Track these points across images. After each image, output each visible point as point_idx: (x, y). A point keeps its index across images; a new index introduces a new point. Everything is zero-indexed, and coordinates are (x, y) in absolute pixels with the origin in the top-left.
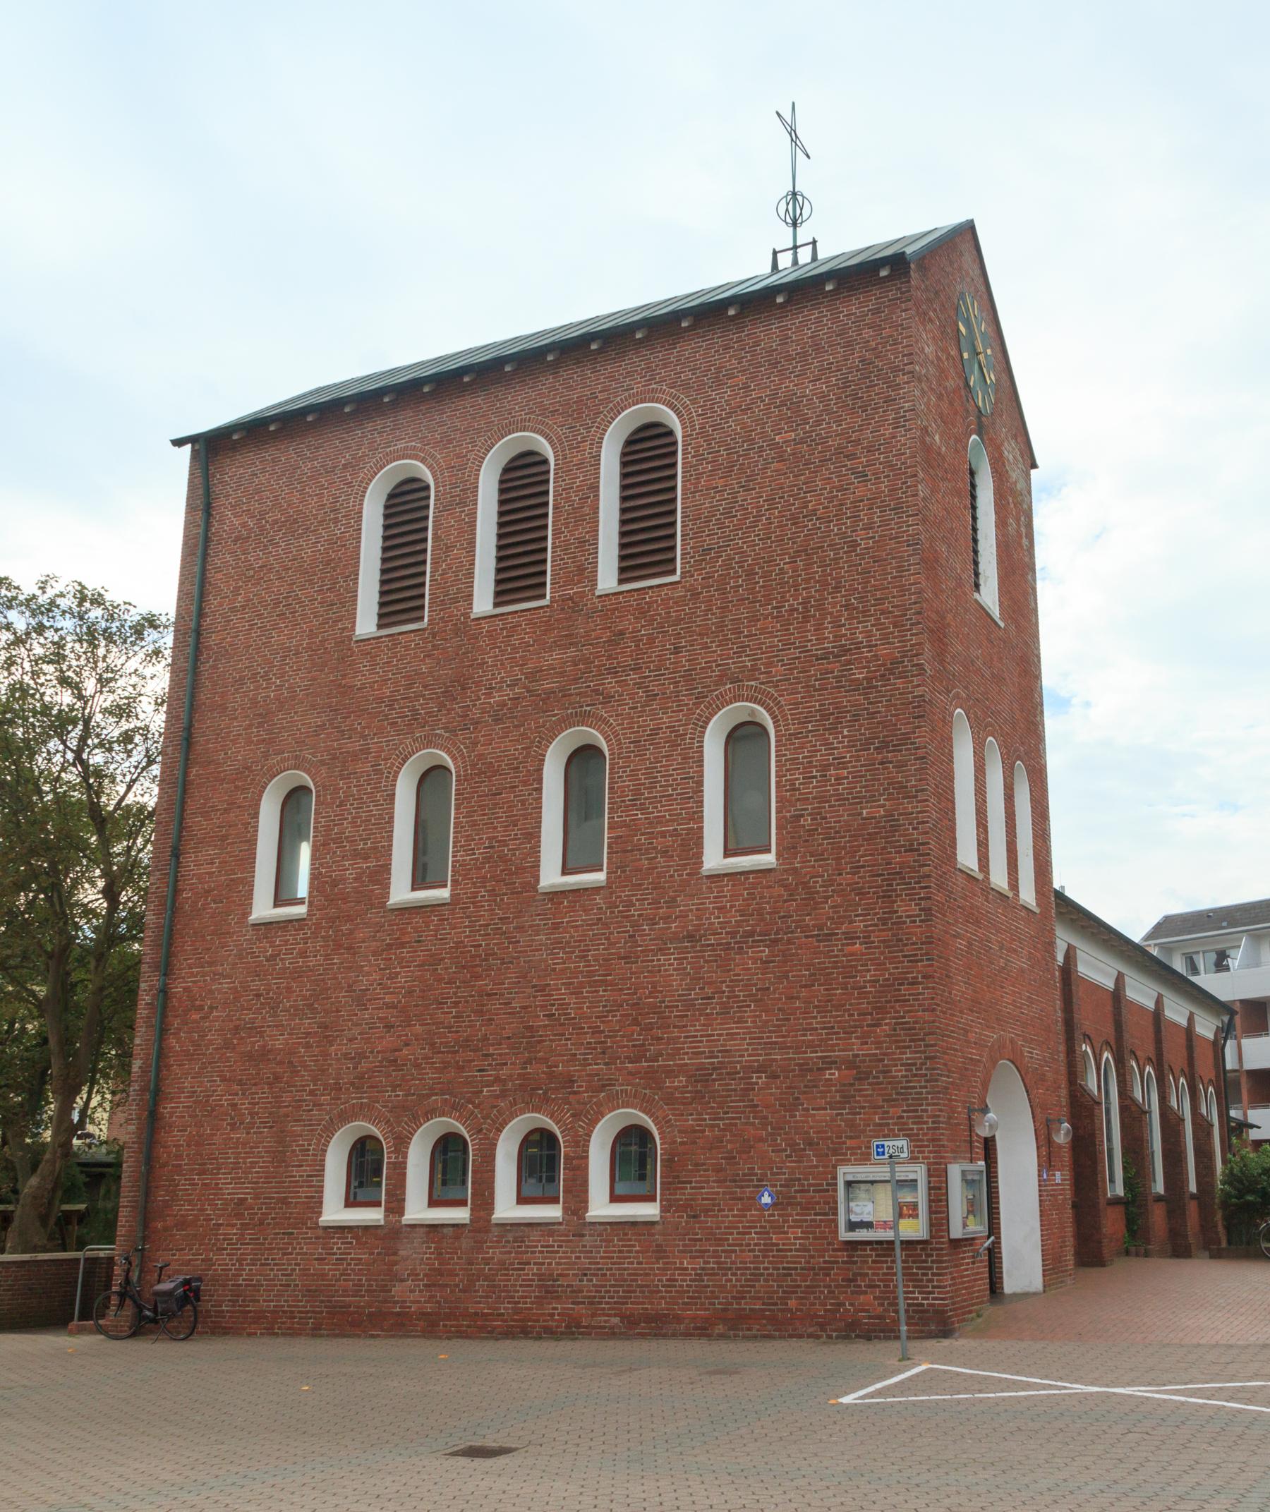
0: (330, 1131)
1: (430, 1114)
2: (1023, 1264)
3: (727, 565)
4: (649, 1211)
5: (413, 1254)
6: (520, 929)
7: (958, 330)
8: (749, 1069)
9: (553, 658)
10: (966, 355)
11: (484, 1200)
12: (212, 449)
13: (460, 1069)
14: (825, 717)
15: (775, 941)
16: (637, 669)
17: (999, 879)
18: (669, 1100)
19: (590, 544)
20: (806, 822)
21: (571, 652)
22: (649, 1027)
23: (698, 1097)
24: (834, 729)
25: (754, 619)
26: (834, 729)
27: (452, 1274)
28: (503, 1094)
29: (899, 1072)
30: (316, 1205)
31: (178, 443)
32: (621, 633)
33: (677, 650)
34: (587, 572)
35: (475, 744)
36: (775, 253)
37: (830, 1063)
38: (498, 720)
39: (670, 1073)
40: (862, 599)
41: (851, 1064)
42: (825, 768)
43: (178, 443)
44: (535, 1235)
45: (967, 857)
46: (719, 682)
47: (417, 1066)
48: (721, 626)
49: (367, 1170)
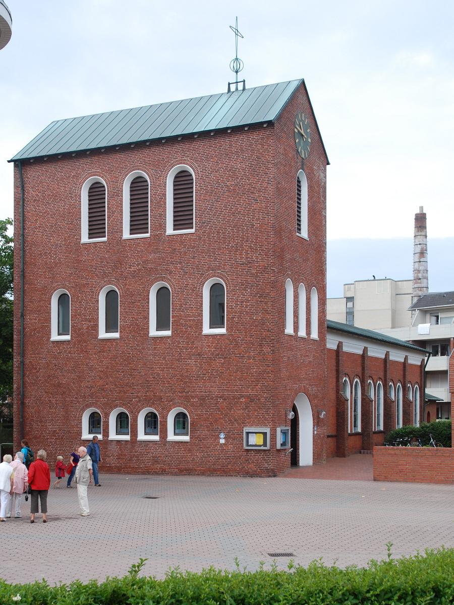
0: (83, 410)
1: (116, 406)
2: (306, 456)
3: (211, 229)
4: (186, 438)
5: (113, 449)
6: (143, 349)
7: (294, 132)
8: (217, 397)
9: (151, 257)
10: (297, 141)
11: (134, 434)
12: (21, 164)
13: (125, 393)
14: (243, 284)
15: (225, 358)
16: (180, 263)
17: (302, 333)
18: (192, 405)
19: (163, 216)
20: (236, 319)
21: (157, 255)
22: (186, 383)
23: (201, 405)
24: (245, 289)
25: (219, 249)
26: (245, 289)
27: (125, 455)
28: (139, 401)
29: (263, 400)
30: (80, 434)
31: (9, 161)
32: (175, 249)
33: (194, 258)
34: (163, 227)
35: (126, 285)
36: (229, 84)
37: (242, 396)
38: (134, 277)
39: (193, 397)
40: (255, 245)
41: (248, 397)
42: (242, 302)
43: (9, 161)
44: (151, 444)
45: (289, 330)
46: (208, 270)
47: (111, 391)
48: (208, 250)
49: (95, 422)
